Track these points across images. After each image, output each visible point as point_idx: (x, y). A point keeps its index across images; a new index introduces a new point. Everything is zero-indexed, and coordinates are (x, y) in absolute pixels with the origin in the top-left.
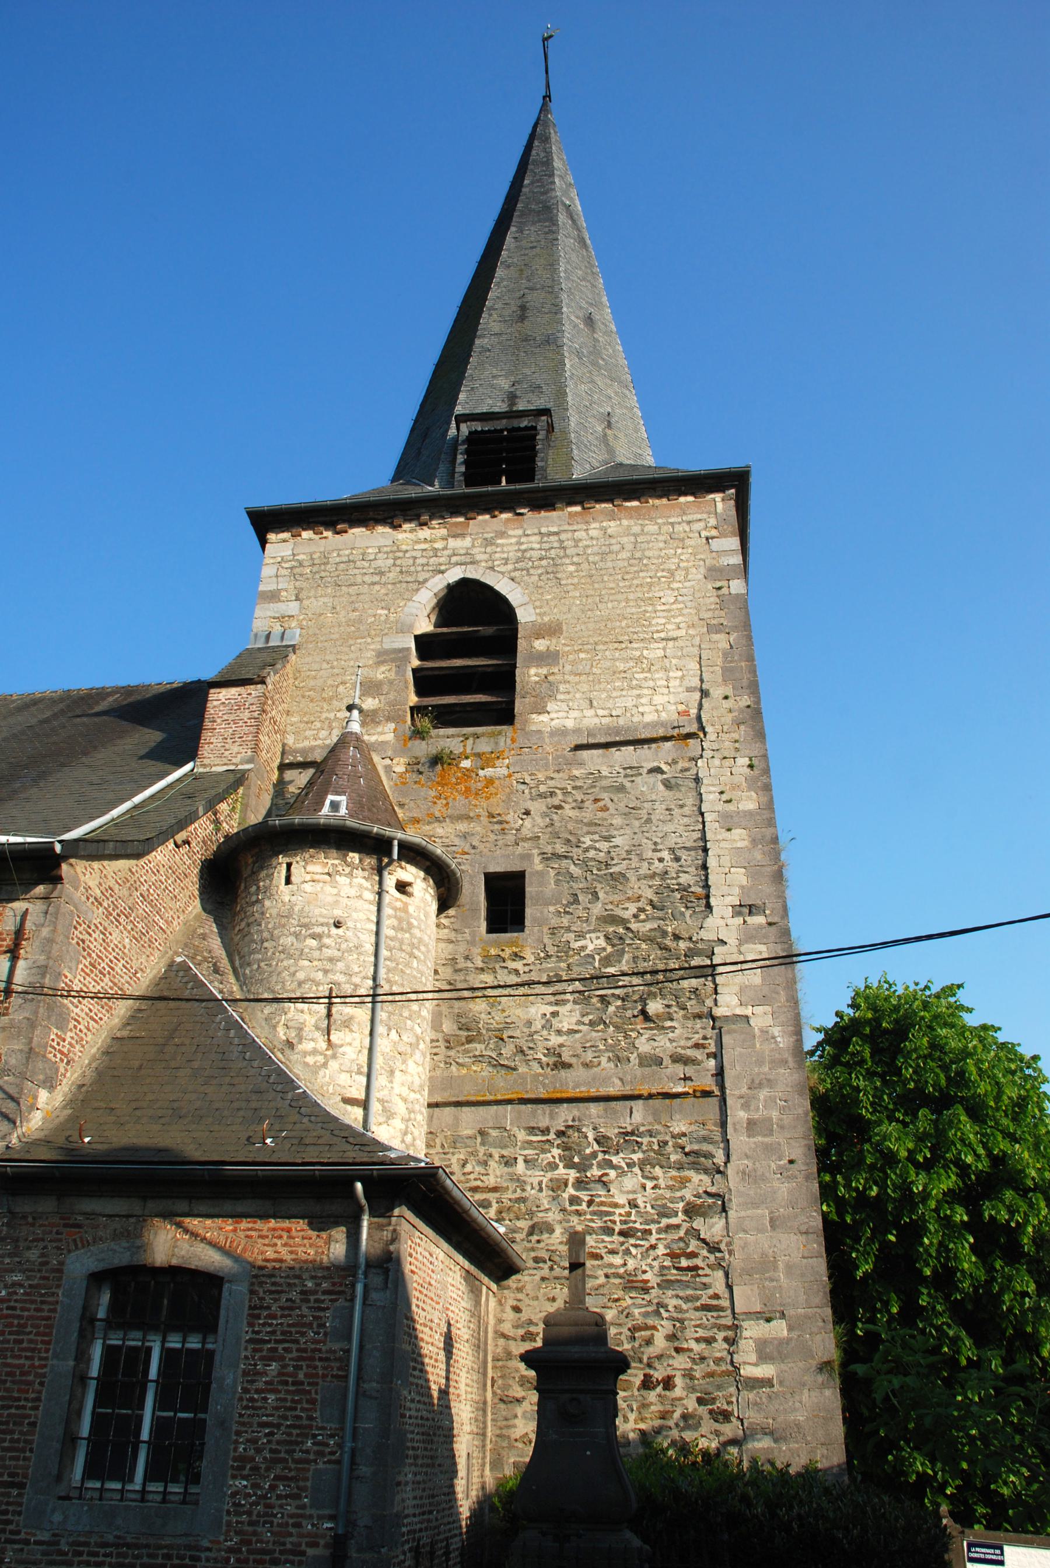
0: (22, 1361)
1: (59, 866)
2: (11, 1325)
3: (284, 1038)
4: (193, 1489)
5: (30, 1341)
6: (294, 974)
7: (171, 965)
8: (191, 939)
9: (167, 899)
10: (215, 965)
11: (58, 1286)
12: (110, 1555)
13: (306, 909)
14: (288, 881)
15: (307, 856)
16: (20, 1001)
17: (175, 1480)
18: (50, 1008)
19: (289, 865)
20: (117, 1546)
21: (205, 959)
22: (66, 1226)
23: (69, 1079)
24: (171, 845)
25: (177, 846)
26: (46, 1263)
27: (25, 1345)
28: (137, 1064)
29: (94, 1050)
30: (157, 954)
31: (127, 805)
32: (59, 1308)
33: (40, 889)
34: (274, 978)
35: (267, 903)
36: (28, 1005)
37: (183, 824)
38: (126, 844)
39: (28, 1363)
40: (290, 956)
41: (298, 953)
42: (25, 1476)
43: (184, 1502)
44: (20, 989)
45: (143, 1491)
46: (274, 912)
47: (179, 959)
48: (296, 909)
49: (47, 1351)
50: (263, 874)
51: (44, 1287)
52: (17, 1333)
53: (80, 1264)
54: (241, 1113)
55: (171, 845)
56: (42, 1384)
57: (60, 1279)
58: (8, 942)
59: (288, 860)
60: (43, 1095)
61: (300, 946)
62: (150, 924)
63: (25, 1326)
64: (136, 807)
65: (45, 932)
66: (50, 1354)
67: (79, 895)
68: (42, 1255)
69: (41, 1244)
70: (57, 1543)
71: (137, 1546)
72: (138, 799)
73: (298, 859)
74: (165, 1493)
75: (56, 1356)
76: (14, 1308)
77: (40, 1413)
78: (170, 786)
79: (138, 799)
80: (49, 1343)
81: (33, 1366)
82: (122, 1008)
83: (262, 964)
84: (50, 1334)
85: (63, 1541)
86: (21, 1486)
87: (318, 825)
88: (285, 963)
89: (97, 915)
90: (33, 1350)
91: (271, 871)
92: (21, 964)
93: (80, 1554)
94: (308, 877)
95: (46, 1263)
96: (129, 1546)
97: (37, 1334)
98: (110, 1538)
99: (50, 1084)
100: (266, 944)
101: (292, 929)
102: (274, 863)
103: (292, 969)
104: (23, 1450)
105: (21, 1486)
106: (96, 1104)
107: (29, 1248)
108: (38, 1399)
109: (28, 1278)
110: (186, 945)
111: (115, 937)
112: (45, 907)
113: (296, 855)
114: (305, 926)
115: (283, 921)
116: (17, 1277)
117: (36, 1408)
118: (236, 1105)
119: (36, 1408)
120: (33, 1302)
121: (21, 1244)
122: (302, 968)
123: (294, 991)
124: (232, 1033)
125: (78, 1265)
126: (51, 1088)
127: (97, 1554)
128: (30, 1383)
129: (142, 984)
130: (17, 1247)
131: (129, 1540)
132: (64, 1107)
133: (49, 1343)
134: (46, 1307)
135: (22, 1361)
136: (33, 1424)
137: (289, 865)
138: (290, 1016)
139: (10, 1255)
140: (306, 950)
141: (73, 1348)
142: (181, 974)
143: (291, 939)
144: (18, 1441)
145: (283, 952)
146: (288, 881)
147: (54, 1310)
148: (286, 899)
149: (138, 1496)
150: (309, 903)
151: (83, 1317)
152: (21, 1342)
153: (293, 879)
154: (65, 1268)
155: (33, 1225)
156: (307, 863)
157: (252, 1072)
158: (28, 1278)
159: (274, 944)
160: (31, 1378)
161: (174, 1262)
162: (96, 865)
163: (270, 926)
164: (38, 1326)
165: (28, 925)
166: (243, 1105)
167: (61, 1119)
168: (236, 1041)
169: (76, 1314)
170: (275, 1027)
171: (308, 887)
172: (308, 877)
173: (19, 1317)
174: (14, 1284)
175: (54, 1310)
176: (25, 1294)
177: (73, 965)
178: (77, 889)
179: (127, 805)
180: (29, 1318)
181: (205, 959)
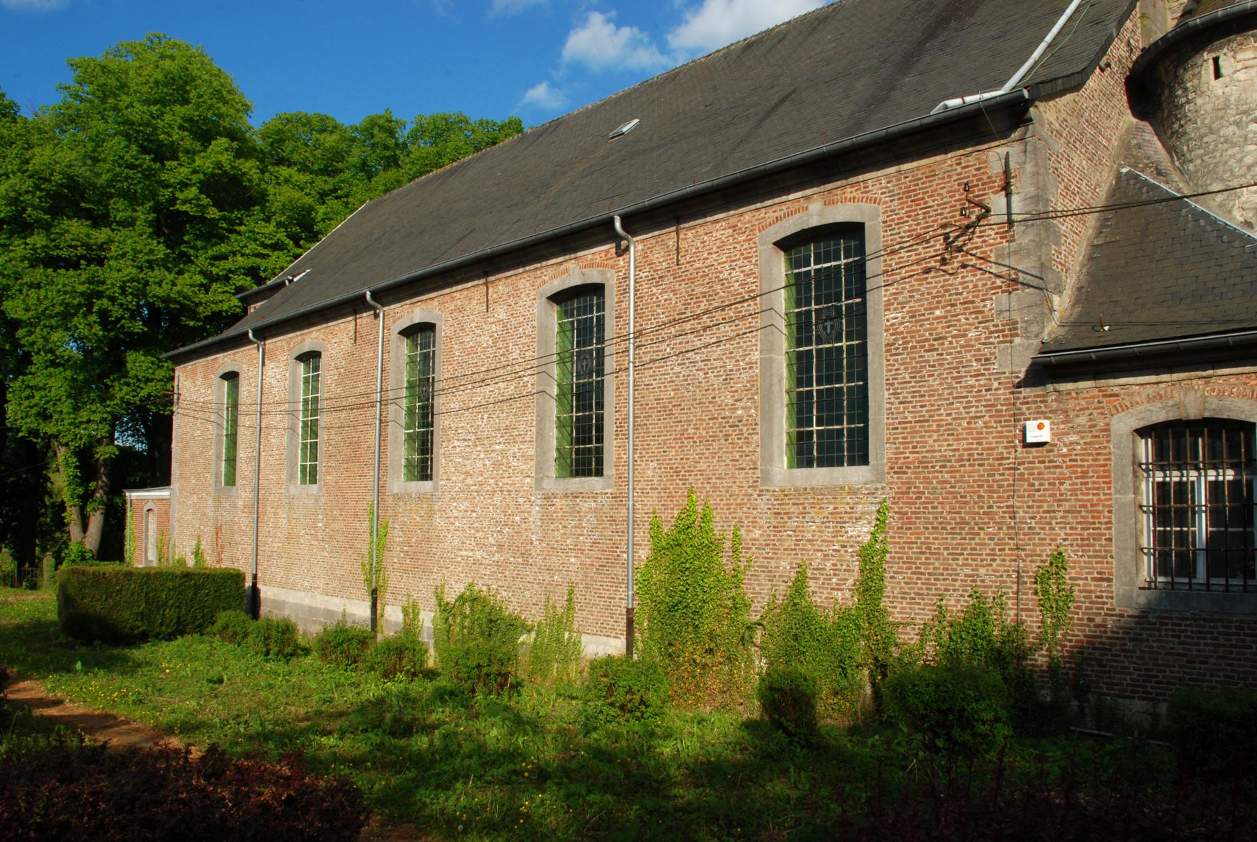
0: (1090, 497)
1: (1027, 110)
2: (1076, 472)
3: (1241, 219)
4: (1250, 582)
5: (1094, 483)
6: (1241, 160)
7: (1119, 176)
8: (1129, 150)
9: (1104, 120)
10: (1156, 169)
11: (1108, 442)
12: (1191, 625)
13: (1243, 96)
14: (1218, 75)
15: (1235, 45)
16: (1022, 228)
17: (1234, 577)
18: (1047, 229)
19: (1216, 60)
20: (1195, 620)
21: (1147, 166)
22: (1104, 396)
23: (1070, 283)
24: (1097, 71)
25: (1102, 70)
26: (1095, 426)
27: (1090, 485)
28: (1122, 262)
29: (1081, 258)
30: (1106, 169)
31: (1042, 47)
32: (1113, 457)
33: (1015, 135)
34: (1221, 169)
35: (1199, 101)
36: (1030, 230)
37: (1103, 50)
38: (1060, 82)
39: (1095, 498)
40: (1234, 145)
41: (1241, 140)
42: (1110, 573)
43: (1245, 591)
44: (1020, 218)
45: (1208, 584)
46: (1209, 107)
47: (1124, 170)
48: (1232, 99)
49: (1109, 488)
50: (1188, 75)
51: (1097, 443)
52: (1082, 477)
53: (1124, 424)
54: (1239, 287)
55: (1097, 71)
56: (1110, 512)
57: (1109, 436)
58: (999, 182)
59: (1214, 55)
60: (1056, 299)
61: (1244, 132)
62: (1097, 144)
63: (1087, 472)
64: (1049, 46)
65: (1029, 168)
66: (1112, 491)
67: (1045, 131)
68: (1091, 420)
69: (1087, 412)
70: (1146, 617)
71: (1212, 620)
72: (1049, 38)
73: (1225, 50)
74: (1227, 585)
75: (1117, 492)
76: (1075, 460)
77: (1113, 531)
78: (1070, 19)
79: (1049, 38)
80: (1109, 482)
81: (1100, 500)
82: (1092, 220)
83: (1205, 158)
84: (1108, 477)
85: (1150, 616)
86: (1109, 580)
87: (1246, 10)
88: (1230, 152)
89: (1059, 145)
90: (1098, 489)
91: (1197, 70)
92: (1015, 198)
93: (1167, 624)
94: (1240, 66)
95: (1095, 426)
96: (1205, 620)
97: (1098, 477)
98: (1189, 615)
99: (1059, 290)
100: (1205, 140)
101: (1232, 119)
102: (1200, 62)
103: (1239, 156)
104: (1105, 557)
105: (1109, 580)
106: (1100, 300)
107: (1078, 416)
108: (1110, 522)
109: (1082, 438)
110: (1126, 157)
111: (1075, 162)
112: (1022, 147)
113: (1221, 48)
114: (1245, 112)
115: (1221, 113)
116: (1074, 438)
117: (1110, 529)
118: (1231, 281)
119: (1110, 529)
120: (1089, 455)
121: (1071, 414)
122: (1249, 153)
123: (1243, 176)
124: (1202, 222)
125: (1121, 424)
126: (1060, 293)
127: (1180, 625)
128: (1099, 512)
129: (1101, 196)
130: (1068, 416)
131: (1204, 616)
132: (1073, 306)
133: (1109, 482)
134: (1101, 457)
135: (1090, 497)
136: (1110, 539)
137: (1216, 60)
138: (1243, 199)
139: (1063, 422)
140: (1250, 135)
141: (1131, 485)
142: (1132, 182)
143: (1232, 129)
144: (1100, 551)
145: (1226, 142)
146: (1218, 75)
147: (1109, 459)
148: (1220, 92)
149: (1205, 587)
150: (1245, 90)
151: (1134, 462)
152: (1086, 483)
153: (1223, 71)
154: (1112, 428)
155: (1076, 399)
156: (1236, 53)
157: (1236, 252)
158: (1082, 438)
159: (1214, 137)
160: (1100, 508)
161: (1207, 415)
162: (1051, 103)
163: (1207, 121)
164: (1098, 472)
165: (1012, 165)
166: (1238, 280)
167: (1075, 315)
168: (1209, 228)
169: (1128, 461)
170: (1230, 212)
171: (1241, 76)
172: (1240, 66)
173: (1081, 466)
174: (1071, 443)
175: (1109, 459)
176: (1083, 449)
177: (1053, 190)
178: (1043, 126)
179: (1042, 47)
180: (1089, 466)
181: (1147, 166)
